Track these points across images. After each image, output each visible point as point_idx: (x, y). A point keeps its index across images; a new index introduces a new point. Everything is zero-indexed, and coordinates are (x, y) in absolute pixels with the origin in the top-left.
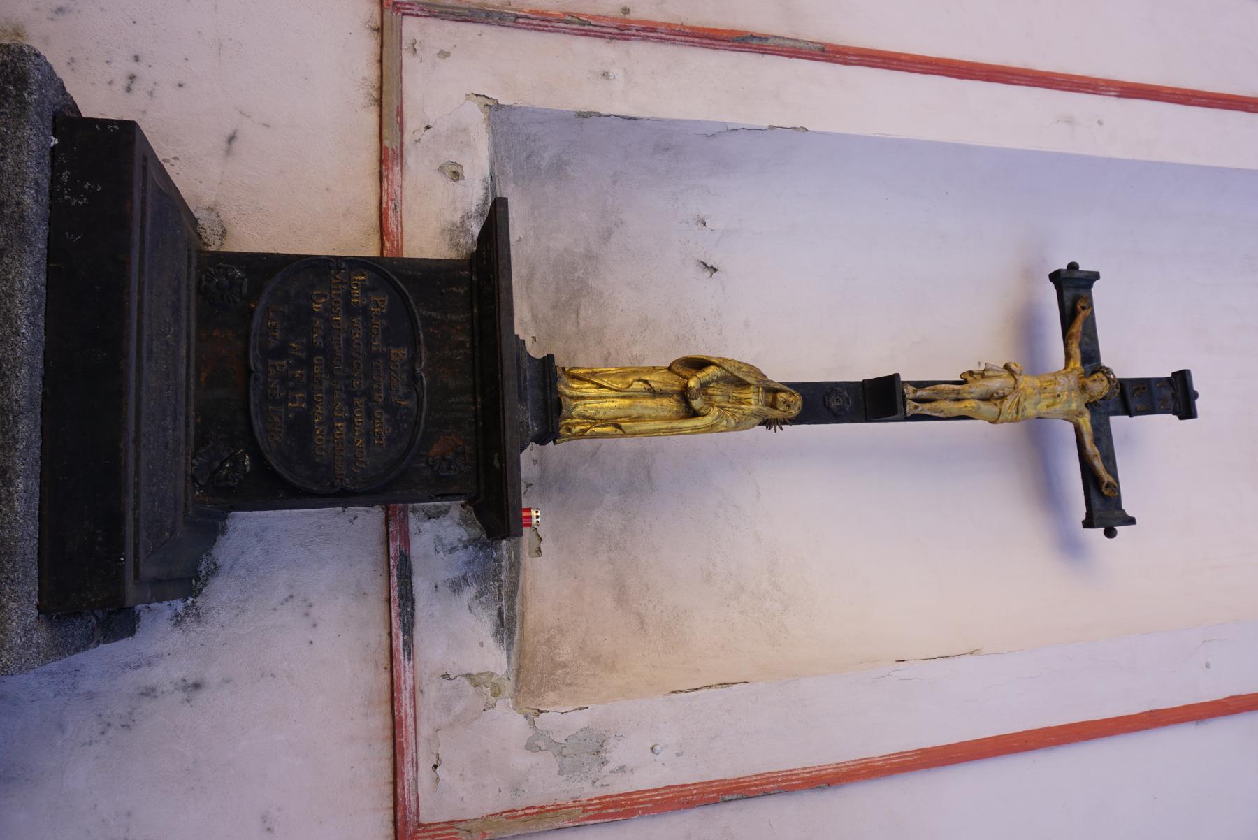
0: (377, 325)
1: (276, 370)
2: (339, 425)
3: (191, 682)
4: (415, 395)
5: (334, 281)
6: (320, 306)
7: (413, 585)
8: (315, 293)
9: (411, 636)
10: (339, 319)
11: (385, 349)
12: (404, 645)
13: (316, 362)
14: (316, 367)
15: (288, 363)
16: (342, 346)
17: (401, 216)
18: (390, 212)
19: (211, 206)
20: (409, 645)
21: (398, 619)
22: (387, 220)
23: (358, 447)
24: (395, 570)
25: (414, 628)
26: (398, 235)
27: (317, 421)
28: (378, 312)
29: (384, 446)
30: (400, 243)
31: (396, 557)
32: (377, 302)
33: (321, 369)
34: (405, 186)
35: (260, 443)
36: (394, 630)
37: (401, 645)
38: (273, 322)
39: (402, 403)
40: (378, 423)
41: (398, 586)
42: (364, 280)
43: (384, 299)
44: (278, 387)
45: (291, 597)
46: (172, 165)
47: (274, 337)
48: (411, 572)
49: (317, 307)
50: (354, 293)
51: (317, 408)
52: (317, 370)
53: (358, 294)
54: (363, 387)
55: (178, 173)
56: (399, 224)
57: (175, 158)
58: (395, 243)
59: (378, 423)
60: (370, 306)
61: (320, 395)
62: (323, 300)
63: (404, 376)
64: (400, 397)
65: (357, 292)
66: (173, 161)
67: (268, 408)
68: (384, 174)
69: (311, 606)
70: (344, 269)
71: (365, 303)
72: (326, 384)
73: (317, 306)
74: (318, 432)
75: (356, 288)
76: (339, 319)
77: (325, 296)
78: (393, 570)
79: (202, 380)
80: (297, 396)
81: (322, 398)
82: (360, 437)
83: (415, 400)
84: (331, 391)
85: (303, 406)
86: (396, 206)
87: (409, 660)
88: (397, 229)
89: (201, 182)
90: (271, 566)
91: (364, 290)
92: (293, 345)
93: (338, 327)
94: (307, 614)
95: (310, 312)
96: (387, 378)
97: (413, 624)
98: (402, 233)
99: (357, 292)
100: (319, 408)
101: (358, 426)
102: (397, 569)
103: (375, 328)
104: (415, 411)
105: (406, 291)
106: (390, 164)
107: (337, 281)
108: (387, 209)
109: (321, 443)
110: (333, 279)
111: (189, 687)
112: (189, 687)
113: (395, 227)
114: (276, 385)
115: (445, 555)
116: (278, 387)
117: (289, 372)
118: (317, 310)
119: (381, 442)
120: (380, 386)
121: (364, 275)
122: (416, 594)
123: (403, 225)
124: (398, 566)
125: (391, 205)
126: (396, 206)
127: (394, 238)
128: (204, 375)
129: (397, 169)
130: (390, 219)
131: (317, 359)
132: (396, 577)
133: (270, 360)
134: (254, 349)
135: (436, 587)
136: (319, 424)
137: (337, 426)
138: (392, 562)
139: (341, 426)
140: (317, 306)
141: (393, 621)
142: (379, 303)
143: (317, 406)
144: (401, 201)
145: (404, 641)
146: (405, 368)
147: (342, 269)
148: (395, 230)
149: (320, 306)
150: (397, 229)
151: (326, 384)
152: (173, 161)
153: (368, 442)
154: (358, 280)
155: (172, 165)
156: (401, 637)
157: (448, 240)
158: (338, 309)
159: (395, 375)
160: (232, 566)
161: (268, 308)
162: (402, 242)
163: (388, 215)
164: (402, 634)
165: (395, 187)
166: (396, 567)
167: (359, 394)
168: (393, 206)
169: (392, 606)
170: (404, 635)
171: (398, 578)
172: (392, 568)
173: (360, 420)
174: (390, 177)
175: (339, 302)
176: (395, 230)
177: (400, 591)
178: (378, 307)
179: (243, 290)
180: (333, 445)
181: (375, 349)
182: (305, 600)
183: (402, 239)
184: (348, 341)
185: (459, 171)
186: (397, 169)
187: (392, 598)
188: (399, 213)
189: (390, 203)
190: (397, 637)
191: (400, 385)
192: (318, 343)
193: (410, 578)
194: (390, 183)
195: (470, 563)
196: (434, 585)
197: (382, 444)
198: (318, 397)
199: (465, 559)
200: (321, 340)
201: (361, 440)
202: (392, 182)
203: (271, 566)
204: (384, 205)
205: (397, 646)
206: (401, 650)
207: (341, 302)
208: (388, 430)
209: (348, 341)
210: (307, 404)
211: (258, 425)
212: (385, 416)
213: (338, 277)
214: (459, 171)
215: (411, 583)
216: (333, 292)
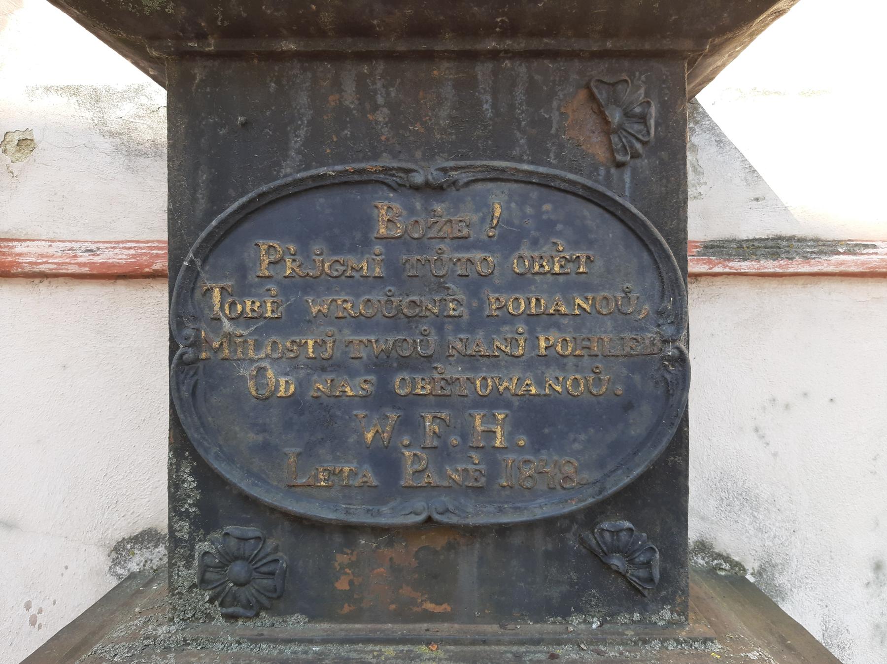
0: (323, 262)
1: (423, 471)
2: (543, 344)
3: (871, 575)
4: (479, 186)
5: (226, 353)
6: (282, 381)
7: (751, 237)
8: (254, 393)
9: (838, 243)
10: (311, 343)
11: (527, 128)
12: (855, 254)
13: (407, 390)
14: (419, 391)
15: (406, 447)
16: (373, 338)
17: (104, 242)
18: (97, 259)
19: (106, 553)
20: (854, 248)
21: (812, 262)
22: (113, 265)
23: (593, 306)
24: (731, 264)
25: (823, 238)
26: (140, 248)
27: (533, 391)
28: (294, 260)
29: (590, 253)
30: (156, 244)
31: (709, 262)
32: (270, 263)
33: (423, 379)
34: (51, 236)
35: (581, 505)
36: (831, 269)
37: (855, 257)
38: (321, 476)
39: (497, 214)
40: (542, 266)
41: (758, 260)
42: (222, 289)
43: (263, 248)
44: (460, 467)
45: (757, 430)
46: (40, 611)
47: (353, 474)
48: (733, 241)
49: (285, 387)
50: (253, 310)
51: (507, 388)
52: (423, 388)
53: (253, 302)
54: (461, 297)
55: (54, 603)
56: (121, 245)
57: (28, 606)
58: (155, 252)
59: (542, 266)
60: (280, 277)
61: (478, 383)
62: (270, 374)
63: (439, 208)
64: (483, 220)
65: (249, 303)
66: (34, 610)
67: (504, 487)
68: (27, 268)
69: (774, 400)
70: (198, 330)
71: (274, 290)
72: (456, 372)
73: (282, 388)
74: (558, 388)
75: (239, 307)
76: (311, 343)
77: (261, 371)
78: (731, 268)
79: (439, 609)
80: (479, 429)
81: (484, 379)
82: (570, 303)
83: (490, 185)
84: (472, 361)
85: (500, 417)
86: (87, 251)
87: (874, 246)
88: (130, 248)
89: (66, 568)
90: (705, 458)
91: (244, 290)
92: (369, 436)
93: (329, 345)
94: (787, 406)
95: (294, 402)
96: (442, 246)
97: (816, 240)
98: (137, 242)
99: (249, 303)
100: (505, 384)
101: (546, 308)
102: (729, 260)
103: (330, 267)
104: (515, 186)
105: (244, 199)
106: (10, 259)
107: (225, 345)
108: (92, 264)
109: (582, 382)
110: (222, 356)
111: (877, 578)
112: (877, 578)
113: (126, 252)
114: (457, 471)
115: (705, 183)
116: (460, 467)
117: (428, 443)
118: (292, 388)
119: (583, 260)
120: (459, 260)
121: (210, 290)
122: (768, 232)
123: (123, 239)
124: (725, 260)
125: (85, 258)
126: (87, 251)
127: (145, 254)
128: (430, 606)
129: (19, 248)
130: (111, 261)
131: (400, 387)
132: (742, 263)
133: (402, 483)
134: (379, 513)
135: (757, 199)
136: (540, 383)
137: (546, 348)
138: (718, 269)
139: (547, 339)
140: (282, 388)
141: (815, 269)
142: (272, 258)
143: (501, 388)
144: (77, 242)
145: (848, 252)
146: (418, 206)
147: (198, 336)
148: (132, 252)
149: (282, 381)
150: (130, 248)
151: (456, 372)
152: (34, 610)
153: (584, 288)
154: (222, 303)
155: (40, 611)
156: (842, 257)
157: (147, 162)
158: (288, 344)
159: (436, 228)
160: (703, 518)
161: (290, 486)
162: (153, 242)
163: (102, 264)
164: (837, 257)
165: (51, 251)
166: (727, 263)
167: (475, 304)
168: (87, 254)
169: (791, 270)
170: (839, 253)
171: (745, 260)
172: (727, 270)
173: (534, 301)
174: (33, 260)
175: (274, 343)
176: (132, 252)
177: (766, 256)
178: (282, 259)
179: (251, 535)
180: (586, 357)
181: (378, 270)
182: (764, 408)
183: (148, 242)
184: (360, 324)
185: (16, 137)
186: (19, 248)
187: (778, 270)
188: (101, 245)
189: (80, 260)
190: (842, 263)
191: (457, 218)
192: (365, 386)
193: (740, 242)
194: (44, 260)
195: (720, 141)
196: (755, 202)
197: (588, 257)
198: (484, 385)
199: (714, 149)
200: (359, 380)
201: (578, 301)
202: (42, 256)
203: (705, 458)
204: (86, 270)
205: (856, 264)
206: (862, 258)
207: (273, 338)
208: (555, 244)
209: (360, 324)
210: (497, 408)
211: (541, 510)
212: (525, 251)
213: (216, 345)
214: (17, 138)
215: (747, 241)
216: (251, 353)
